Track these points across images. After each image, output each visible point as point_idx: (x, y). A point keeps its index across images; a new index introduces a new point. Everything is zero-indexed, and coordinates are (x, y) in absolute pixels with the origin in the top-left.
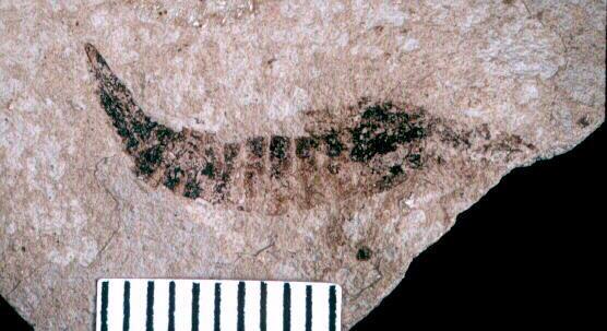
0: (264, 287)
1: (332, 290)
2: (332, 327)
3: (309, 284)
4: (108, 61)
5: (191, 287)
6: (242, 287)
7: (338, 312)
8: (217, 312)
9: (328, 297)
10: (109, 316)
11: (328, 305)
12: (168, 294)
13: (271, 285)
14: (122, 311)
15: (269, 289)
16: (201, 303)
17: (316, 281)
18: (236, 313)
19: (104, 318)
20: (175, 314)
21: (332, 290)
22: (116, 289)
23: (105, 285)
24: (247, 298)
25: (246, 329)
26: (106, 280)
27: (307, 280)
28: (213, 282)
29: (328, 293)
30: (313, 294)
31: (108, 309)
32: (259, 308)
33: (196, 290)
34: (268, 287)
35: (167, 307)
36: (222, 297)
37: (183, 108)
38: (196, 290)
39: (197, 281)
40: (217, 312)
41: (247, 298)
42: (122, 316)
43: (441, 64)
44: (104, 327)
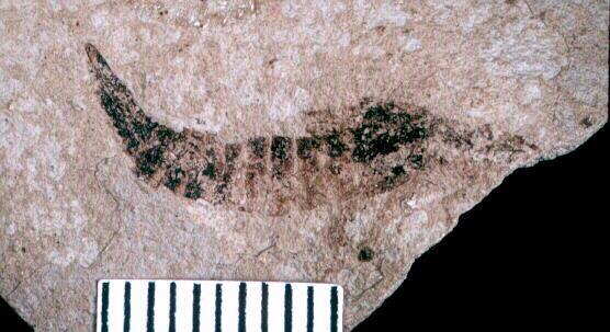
0: (265, 288)
1: (334, 291)
2: (127, 327)
3: (310, 285)
4: (108, 61)
5: (192, 288)
6: (243, 288)
7: (340, 313)
8: (218, 313)
9: (330, 298)
10: (110, 317)
11: (330, 306)
12: (169, 295)
13: (272, 286)
14: (123, 312)
15: (270, 290)
16: (202, 304)
17: (317, 281)
18: (237, 314)
19: (105, 319)
20: (176, 315)
21: (334, 291)
22: (117, 290)
23: (106, 286)
24: (248, 299)
25: (248, 330)
26: (106, 281)
27: (309, 281)
28: (214, 283)
29: (330, 293)
30: (315, 295)
31: (109, 310)
32: (260, 308)
33: (197, 291)
34: (269, 288)
35: (168, 308)
36: (223, 298)
37: (183, 109)
38: (197, 291)
39: (198, 282)
40: (218, 313)
41: (248, 299)
42: (122, 317)
43: (443, 64)
44: (105, 328)
